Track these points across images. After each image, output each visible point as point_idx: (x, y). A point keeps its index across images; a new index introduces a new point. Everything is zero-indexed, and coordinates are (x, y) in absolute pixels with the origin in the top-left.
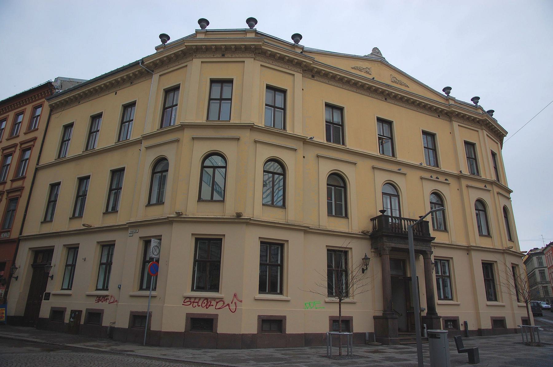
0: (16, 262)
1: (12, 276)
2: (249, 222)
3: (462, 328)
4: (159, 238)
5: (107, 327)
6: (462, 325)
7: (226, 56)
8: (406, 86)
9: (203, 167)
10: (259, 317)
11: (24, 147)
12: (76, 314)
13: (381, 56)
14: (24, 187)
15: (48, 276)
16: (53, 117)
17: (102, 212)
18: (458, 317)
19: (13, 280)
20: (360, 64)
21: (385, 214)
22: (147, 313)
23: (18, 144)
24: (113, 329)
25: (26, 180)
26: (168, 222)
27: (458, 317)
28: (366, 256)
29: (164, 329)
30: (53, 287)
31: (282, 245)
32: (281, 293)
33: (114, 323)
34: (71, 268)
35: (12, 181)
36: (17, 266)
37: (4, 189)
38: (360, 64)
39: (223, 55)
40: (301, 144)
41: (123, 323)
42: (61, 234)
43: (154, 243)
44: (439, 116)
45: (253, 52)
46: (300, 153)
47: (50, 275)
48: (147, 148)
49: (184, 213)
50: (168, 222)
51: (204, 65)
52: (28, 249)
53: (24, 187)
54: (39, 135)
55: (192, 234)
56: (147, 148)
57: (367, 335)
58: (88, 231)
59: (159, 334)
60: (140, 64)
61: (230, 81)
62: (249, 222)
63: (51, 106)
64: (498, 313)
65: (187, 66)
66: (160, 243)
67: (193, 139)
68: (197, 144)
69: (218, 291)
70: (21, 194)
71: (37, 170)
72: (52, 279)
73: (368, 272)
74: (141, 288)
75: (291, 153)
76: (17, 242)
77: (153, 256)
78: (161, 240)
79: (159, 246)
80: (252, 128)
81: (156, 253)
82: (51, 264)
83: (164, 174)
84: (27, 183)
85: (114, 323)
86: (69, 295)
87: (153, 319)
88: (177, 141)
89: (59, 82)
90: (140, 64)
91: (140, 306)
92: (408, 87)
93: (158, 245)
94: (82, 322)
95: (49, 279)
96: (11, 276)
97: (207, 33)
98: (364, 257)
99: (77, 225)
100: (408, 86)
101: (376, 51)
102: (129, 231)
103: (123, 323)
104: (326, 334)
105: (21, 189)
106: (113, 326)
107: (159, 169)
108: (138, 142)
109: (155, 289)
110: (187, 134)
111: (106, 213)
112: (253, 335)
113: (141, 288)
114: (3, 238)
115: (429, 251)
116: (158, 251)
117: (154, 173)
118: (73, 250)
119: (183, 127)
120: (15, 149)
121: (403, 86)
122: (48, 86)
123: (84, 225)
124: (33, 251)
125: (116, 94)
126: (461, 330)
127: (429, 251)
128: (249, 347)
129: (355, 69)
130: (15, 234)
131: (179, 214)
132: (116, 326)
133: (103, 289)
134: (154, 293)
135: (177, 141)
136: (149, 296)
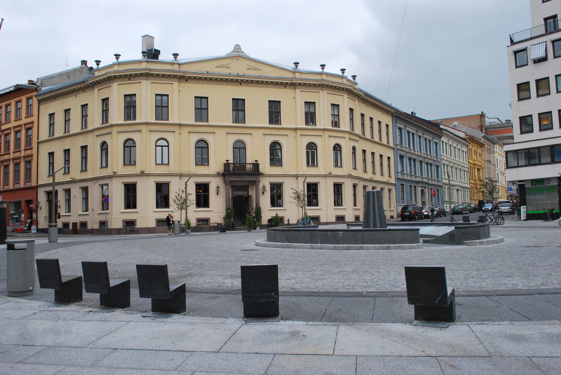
0: (38, 199)
1: (38, 207)
2: (148, 175)
3: (286, 223)
4: (107, 185)
5: (90, 229)
6: (286, 221)
7: (131, 79)
8: (259, 70)
9: (125, 147)
10: (156, 219)
11: (27, 127)
12: (75, 224)
14: (33, 155)
15: (58, 206)
16: (41, 107)
19: (39, 209)
21: (229, 162)
22: (105, 221)
23: (22, 125)
24: (93, 230)
25: (33, 149)
26: (110, 177)
29: (113, 228)
30: (62, 211)
31: (168, 184)
32: (342, 206)
33: (93, 227)
34: (68, 201)
35: (25, 150)
36: (40, 202)
37: (20, 155)
38: (224, 62)
39: (129, 79)
40: (178, 127)
41: (97, 226)
43: (105, 187)
44: (285, 87)
45: (146, 76)
46: (177, 133)
47: (58, 205)
48: (97, 136)
49: (117, 172)
50: (110, 177)
51: (120, 86)
53: (33, 155)
54: (34, 119)
55: (122, 182)
56: (97, 136)
58: (73, 181)
59: (111, 230)
60: (86, 82)
61: (135, 95)
62: (148, 175)
63: (38, 100)
64: (340, 213)
65: (111, 86)
66: (108, 188)
67: (118, 132)
68: (120, 135)
69: (169, 208)
70: (32, 158)
71: (38, 143)
72: (60, 208)
74: (103, 209)
75: (172, 134)
76: (36, 188)
77: (105, 194)
78: (108, 185)
79: (107, 189)
80: (147, 124)
81: (106, 193)
82: (57, 200)
83: (107, 150)
84: (34, 152)
85: (93, 227)
86: (70, 215)
87: (109, 223)
88: (110, 133)
89: (40, 81)
90: (86, 82)
91: (102, 218)
93: (107, 189)
94: (78, 228)
95: (58, 207)
96: (37, 207)
97: (120, 64)
98: (217, 187)
99: (67, 178)
101: (237, 48)
102: (94, 181)
103: (97, 226)
104: (222, 223)
105: (31, 156)
106: (92, 228)
107: (104, 148)
108: (92, 131)
109: (108, 209)
110: (115, 130)
111: (82, 171)
112: (154, 228)
113: (103, 209)
114: (27, 186)
115: (258, 181)
116: (107, 191)
117: (102, 150)
118: (68, 191)
119: (112, 126)
120: (22, 128)
121: (257, 70)
123: (71, 178)
124: (46, 193)
125: (76, 97)
127: (258, 181)
128: (152, 233)
130: (34, 184)
131: (115, 173)
132: (94, 228)
133: (86, 211)
134: (108, 211)
135: (110, 133)
136: (105, 213)
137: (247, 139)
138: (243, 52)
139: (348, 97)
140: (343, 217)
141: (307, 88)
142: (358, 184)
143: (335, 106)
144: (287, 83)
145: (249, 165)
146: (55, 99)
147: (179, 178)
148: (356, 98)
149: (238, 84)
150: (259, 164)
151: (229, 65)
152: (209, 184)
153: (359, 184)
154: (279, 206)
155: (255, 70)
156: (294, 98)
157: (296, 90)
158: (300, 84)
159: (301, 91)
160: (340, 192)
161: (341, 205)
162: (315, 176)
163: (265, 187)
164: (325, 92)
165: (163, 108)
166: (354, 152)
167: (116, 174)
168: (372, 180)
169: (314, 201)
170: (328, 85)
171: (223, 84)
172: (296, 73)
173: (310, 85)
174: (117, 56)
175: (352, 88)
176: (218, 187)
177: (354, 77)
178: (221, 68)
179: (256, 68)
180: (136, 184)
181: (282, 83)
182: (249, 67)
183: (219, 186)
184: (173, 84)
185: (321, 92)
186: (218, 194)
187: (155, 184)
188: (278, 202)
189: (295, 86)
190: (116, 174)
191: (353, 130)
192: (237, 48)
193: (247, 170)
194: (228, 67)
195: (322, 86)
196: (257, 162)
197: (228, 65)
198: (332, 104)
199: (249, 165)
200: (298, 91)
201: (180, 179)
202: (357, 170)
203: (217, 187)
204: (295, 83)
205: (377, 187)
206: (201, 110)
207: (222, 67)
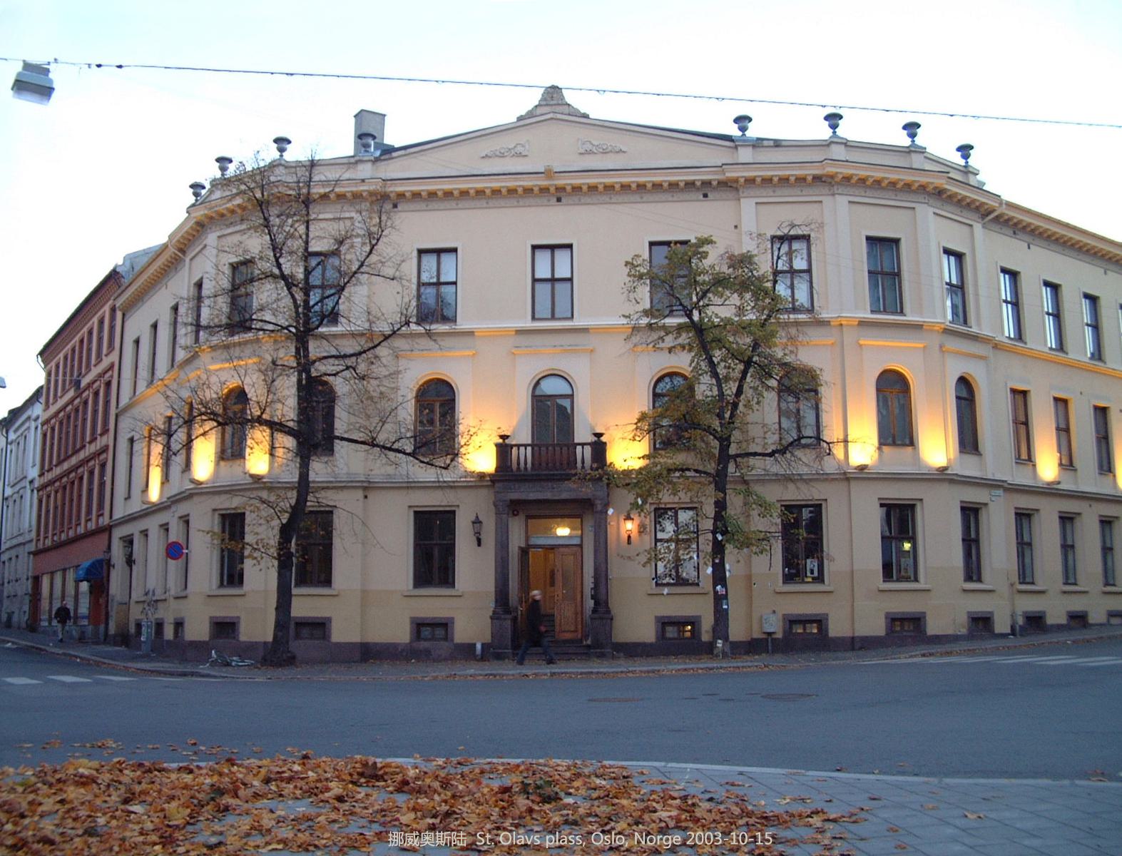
13: (45, 387)
17: (141, 489)
18: (1044, 612)
20: (508, 142)
27: (1044, 612)
28: (477, 517)
38: (508, 142)
42: (1085, 316)
44: (705, 196)
52: (157, 527)
57: (479, 646)
64: (980, 605)
73: (626, 536)
76: (109, 529)
91: (223, 611)
92: (624, 152)
98: (473, 518)
100: (623, 149)
101: (553, 94)
104: (474, 645)
121: (611, 154)
122: (113, 277)
126: (703, 639)
129: (490, 157)
130: (105, 521)
137: (577, 368)
138: (569, 105)
139: (934, 213)
140: (919, 619)
141: (779, 192)
142: (986, 504)
143: (883, 246)
144: (707, 184)
145: (522, 449)
146: (176, 268)
147: (360, 494)
148: (975, 216)
149: (549, 201)
150: (605, 443)
151: (523, 146)
152: (821, 505)
153: (991, 506)
154: (903, 577)
155: (605, 152)
156: (736, 227)
157: (742, 200)
158: (750, 181)
159: (850, 202)
160: (911, 534)
161: (912, 578)
162: (909, 479)
163: (480, 522)
164: (842, 201)
165: (549, 276)
166: (964, 394)
167: (866, 471)
168: (1057, 489)
169: (811, 564)
170: (847, 179)
171: (448, 207)
172: (739, 148)
173: (784, 181)
174: (282, 142)
175: (944, 181)
176: (477, 522)
177: (965, 150)
178: (497, 159)
179: (610, 148)
180: (912, 507)
181: (690, 185)
182: (588, 147)
183: (481, 519)
184: (821, 202)
185: (827, 200)
186: (479, 544)
187: (412, 514)
188: (808, 569)
189: (737, 189)
190: (866, 471)
191: (965, 322)
192: (553, 94)
193: (579, 464)
194: (520, 155)
195: (829, 180)
196: (507, 441)
197: (519, 149)
198: (869, 238)
199: (522, 449)
200: (748, 205)
201: (366, 497)
202: (981, 455)
203: (474, 523)
204: (736, 180)
205: (1042, 512)
206: (791, 267)
207: (502, 156)
